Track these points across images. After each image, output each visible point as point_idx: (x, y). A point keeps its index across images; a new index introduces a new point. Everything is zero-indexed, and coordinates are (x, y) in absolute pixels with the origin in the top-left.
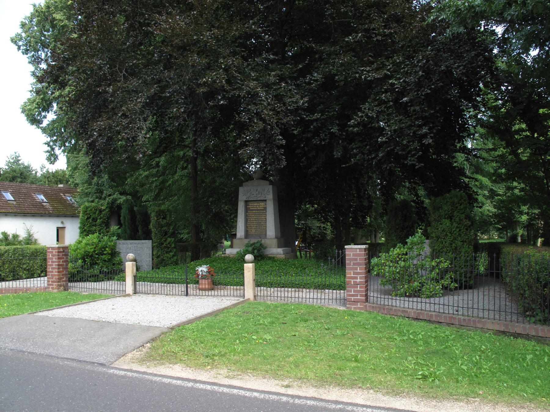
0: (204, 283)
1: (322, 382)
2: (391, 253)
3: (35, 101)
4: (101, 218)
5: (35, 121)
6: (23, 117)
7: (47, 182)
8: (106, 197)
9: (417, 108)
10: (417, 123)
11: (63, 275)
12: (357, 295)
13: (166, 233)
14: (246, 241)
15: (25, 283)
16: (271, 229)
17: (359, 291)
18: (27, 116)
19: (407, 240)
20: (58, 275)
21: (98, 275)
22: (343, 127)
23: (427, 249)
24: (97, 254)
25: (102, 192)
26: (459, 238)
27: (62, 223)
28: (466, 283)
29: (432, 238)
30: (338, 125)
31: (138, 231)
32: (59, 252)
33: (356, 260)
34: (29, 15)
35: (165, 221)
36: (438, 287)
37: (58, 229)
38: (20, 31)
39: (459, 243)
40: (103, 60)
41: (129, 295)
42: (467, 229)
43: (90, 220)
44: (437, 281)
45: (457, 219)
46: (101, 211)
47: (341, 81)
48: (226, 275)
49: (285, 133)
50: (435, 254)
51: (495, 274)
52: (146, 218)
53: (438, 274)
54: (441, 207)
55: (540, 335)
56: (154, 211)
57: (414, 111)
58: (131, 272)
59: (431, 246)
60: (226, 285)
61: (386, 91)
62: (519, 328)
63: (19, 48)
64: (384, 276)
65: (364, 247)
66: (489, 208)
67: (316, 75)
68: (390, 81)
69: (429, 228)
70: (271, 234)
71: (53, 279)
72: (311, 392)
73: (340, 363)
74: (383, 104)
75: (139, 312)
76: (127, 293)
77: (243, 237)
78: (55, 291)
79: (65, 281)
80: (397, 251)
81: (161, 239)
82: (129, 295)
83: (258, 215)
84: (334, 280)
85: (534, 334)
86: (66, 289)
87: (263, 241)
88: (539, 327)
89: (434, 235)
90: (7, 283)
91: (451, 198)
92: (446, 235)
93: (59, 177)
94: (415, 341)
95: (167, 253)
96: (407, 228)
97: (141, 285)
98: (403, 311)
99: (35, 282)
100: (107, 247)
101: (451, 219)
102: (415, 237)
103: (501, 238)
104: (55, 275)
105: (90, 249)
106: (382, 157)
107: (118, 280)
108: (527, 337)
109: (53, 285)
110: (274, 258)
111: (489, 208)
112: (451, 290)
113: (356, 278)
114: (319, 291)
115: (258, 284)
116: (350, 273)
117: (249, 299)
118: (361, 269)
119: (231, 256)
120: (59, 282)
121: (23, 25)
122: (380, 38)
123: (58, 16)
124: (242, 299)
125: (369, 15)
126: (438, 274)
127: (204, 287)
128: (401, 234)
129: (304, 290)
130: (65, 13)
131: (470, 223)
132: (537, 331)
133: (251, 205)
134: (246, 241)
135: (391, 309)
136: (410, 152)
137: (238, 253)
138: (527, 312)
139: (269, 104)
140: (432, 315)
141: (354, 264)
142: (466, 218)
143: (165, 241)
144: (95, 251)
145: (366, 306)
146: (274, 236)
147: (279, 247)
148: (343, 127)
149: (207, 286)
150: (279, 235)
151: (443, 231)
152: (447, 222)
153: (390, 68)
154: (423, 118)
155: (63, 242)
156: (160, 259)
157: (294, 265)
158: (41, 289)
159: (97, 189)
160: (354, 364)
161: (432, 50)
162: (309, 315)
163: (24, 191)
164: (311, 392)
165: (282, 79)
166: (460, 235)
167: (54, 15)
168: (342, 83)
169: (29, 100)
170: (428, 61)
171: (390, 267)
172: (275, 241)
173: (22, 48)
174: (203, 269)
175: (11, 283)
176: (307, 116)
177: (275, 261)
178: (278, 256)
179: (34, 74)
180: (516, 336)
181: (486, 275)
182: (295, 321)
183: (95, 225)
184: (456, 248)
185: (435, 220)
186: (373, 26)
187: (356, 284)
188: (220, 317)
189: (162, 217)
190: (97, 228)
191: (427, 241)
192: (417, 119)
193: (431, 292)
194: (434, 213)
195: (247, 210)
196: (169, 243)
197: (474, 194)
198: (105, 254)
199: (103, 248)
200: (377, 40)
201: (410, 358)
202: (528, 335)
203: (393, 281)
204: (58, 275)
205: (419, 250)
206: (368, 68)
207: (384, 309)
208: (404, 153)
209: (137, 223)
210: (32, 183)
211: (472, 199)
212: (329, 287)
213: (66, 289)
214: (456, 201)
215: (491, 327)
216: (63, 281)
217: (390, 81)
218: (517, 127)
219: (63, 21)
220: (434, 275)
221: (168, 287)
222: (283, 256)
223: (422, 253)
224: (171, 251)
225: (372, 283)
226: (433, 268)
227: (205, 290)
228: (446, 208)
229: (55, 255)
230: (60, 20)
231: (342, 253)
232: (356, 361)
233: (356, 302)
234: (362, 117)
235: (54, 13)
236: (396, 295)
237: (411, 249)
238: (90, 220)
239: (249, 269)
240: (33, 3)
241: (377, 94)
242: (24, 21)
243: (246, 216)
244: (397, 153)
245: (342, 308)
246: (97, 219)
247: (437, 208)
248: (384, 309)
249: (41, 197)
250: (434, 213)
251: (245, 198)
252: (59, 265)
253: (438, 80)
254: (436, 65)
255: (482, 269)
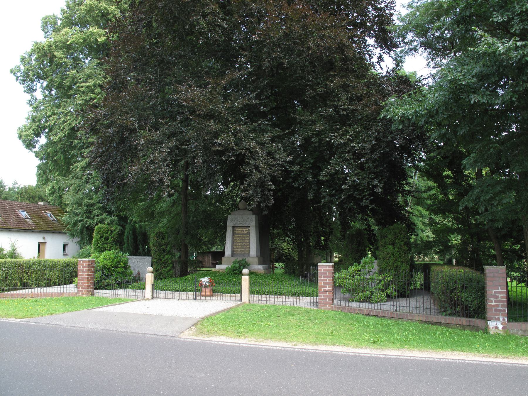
0: (206, 291)
1: (315, 343)
2: (349, 270)
3: (31, 127)
4: (112, 238)
5: (30, 145)
6: (20, 143)
7: (20, 198)
8: (94, 217)
9: (371, 165)
10: (370, 176)
11: (91, 283)
12: (326, 299)
13: (164, 251)
14: (233, 259)
15: (56, 289)
16: (253, 250)
17: (328, 296)
18: (24, 142)
19: (361, 261)
20: (88, 283)
21: (113, 284)
22: (315, 176)
23: (376, 267)
24: (113, 267)
25: (90, 212)
26: (400, 259)
27: (44, 238)
28: (404, 293)
29: (380, 259)
30: (312, 173)
31: (138, 249)
32: (89, 265)
33: (326, 273)
34: (29, 50)
35: (164, 241)
36: (384, 295)
37: (65, 246)
38: (18, 63)
39: (400, 263)
40: (135, 118)
41: (148, 299)
42: (405, 253)
43: (103, 239)
44: (383, 291)
45: (398, 245)
46: (112, 232)
47: (316, 142)
48: (228, 283)
49: (274, 179)
50: (381, 272)
51: (426, 288)
52: (145, 238)
53: (383, 285)
54: (386, 236)
55: (447, 322)
56: (154, 232)
57: (368, 167)
58: (150, 281)
59: (379, 265)
60: (223, 292)
61: (349, 152)
62: (435, 319)
63: (17, 79)
64: (344, 287)
65: (332, 264)
66: (428, 234)
67: (297, 136)
68: (352, 145)
69: (377, 252)
70: (253, 254)
71: (83, 286)
72: (310, 347)
73: (322, 337)
74: (346, 161)
75: (160, 312)
76: (146, 297)
77: (230, 256)
78: (85, 296)
79: (92, 288)
80: (354, 268)
81: (160, 256)
82: (148, 299)
83: (242, 237)
84: (307, 289)
85: (444, 322)
86: (92, 295)
87: (247, 260)
88: (447, 317)
89: (381, 257)
90: (33, 289)
91: (394, 229)
92: (390, 257)
93: (32, 194)
94: (368, 326)
95: (164, 267)
96: (360, 251)
97: (157, 293)
98: (359, 310)
99: (62, 289)
100: (121, 262)
101: (394, 245)
102: (367, 258)
103: (441, 260)
104: (85, 283)
105: (108, 263)
106: (344, 198)
107: (132, 288)
108: (440, 324)
109: (82, 291)
110: (255, 273)
111: (428, 234)
112: (392, 298)
113: (326, 287)
114: (295, 297)
115: (251, 292)
116: (321, 283)
117: (245, 302)
118: (329, 281)
119: (220, 271)
120: (88, 288)
121: (23, 59)
122: (345, 113)
123: (58, 54)
124: (239, 303)
125: (337, 95)
126: (383, 285)
127: (207, 294)
128: (357, 255)
129: (284, 297)
130: (64, 51)
131: (407, 248)
132: (445, 320)
133: (237, 230)
134: (233, 259)
135: (351, 309)
136: (364, 196)
137: (227, 268)
138: (443, 310)
139: (264, 159)
140: (379, 312)
141: (324, 277)
142: (404, 245)
143: (163, 257)
144: (111, 265)
145: (332, 307)
146: (256, 256)
147: (259, 264)
148: (315, 176)
149: (209, 294)
150: (259, 254)
151: (388, 254)
152: (391, 247)
153: (352, 135)
154: (374, 173)
155: (44, 256)
156: (159, 272)
157: (273, 278)
158: (72, 294)
159: (87, 210)
160: (331, 337)
161: (382, 126)
162: (293, 312)
163: (9, 207)
164: (310, 347)
165: (273, 140)
166: (400, 257)
167: (55, 53)
168: (317, 144)
169: (25, 126)
170: (378, 134)
171: (349, 279)
172: (256, 260)
173: (20, 78)
174: (205, 280)
175: (36, 289)
176: (290, 167)
177: (257, 275)
178: (259, 271)
179: (30, 103)
180: (433, 323)
181: (422, 289)
182: (285, 315)
183: (107, 243)
184: (397, 267)
185: (382, 245)
186: (340, 103)
187: (326, 291)
188: (232, 312)
189: (161, 237)
190: (109, 246)
191: (376, 261)
192: (370, 173)
193: (378, 299)
194: (381, 240)
195: (233, 234)
196: (166, 260)
197: (412, 225)
198: (120, 267)
199: (118, 262)
200: (343, 114)
201: (365, 334)
202: (440, 323)
203: (351, 291)
204: (88, 283)
205: (369, 267)
206: (336, 134)
207: (345, 309)
208: (360, 197)
209: (138, 241)
210: (6, 199)
211: (411, 227)
212: (303, 294)
213: (92, 295)
214: (398, 231)
215: (417, 318)
216: (90, 288)
217: (352, 145)
218: (445, 173)
219: (62, 59)
220: (380, 286)
221: (177, 294)
222: (263, 272)
223: (372, 270)
224: (168, 266)
225: (337, 293)
226: (380, 281)
227: (208, 296)
228: (390, 237)
229: (85, 267)
230: (60, 58)
231: (315, 269)
232: (332, 335)
233: (325, 304)
234: (331, 169)
235: (55, 51)
236: (353, 301)
237: (364, 267)
238: (103, 239)
239: (245, 280)
240: (35, 41)
241: (342, 153)
242: (24, 55)
243: (233, 239)
244: (355, 197)
245: (315, 309)
246: (108, 238)
247: (384, 237)
248: (345, 309)
249: (24, 214)
250: (381, 240)
251: (232, 224)
252: (88, 275)
253: (386, 147)
254: (384, 137)
255: (418, 285)
